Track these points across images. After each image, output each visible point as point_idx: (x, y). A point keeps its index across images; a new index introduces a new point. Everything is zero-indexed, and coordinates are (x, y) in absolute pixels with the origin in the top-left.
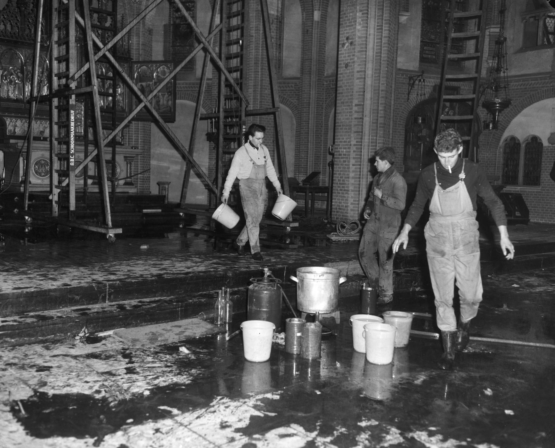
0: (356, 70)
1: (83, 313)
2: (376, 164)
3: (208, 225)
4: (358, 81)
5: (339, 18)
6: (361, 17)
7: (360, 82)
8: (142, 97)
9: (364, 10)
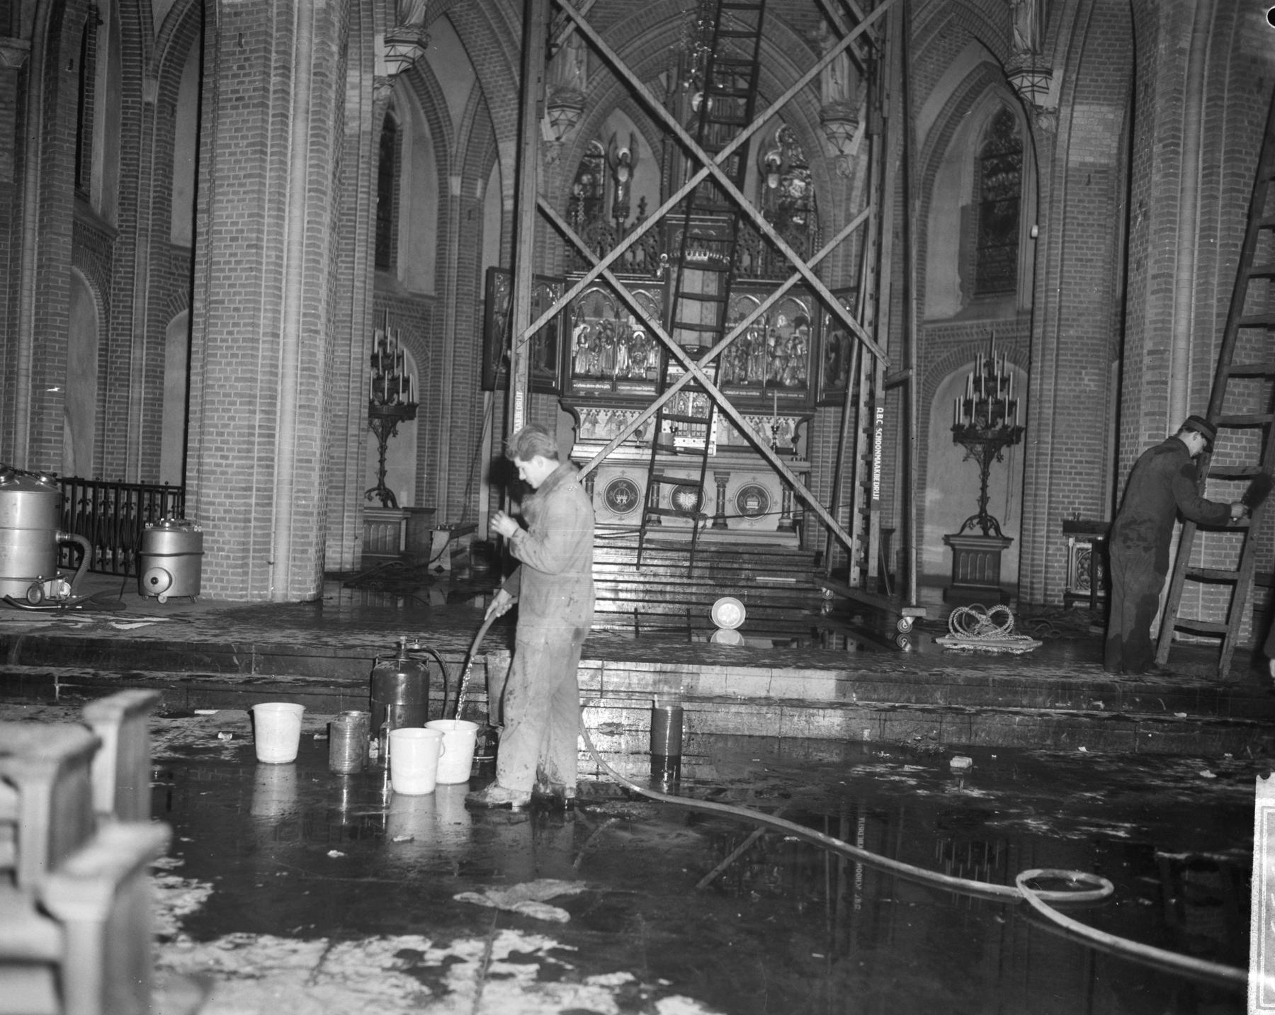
0: (1151, 272)
1: (892, 531)
2: (522, 477)
3: (797, 526)
4: (1153, 297)
5: (1134, 29)
6: (1163, 154)
7: (1157, 299)
8: (701, 155)
9: (1165, 139)
